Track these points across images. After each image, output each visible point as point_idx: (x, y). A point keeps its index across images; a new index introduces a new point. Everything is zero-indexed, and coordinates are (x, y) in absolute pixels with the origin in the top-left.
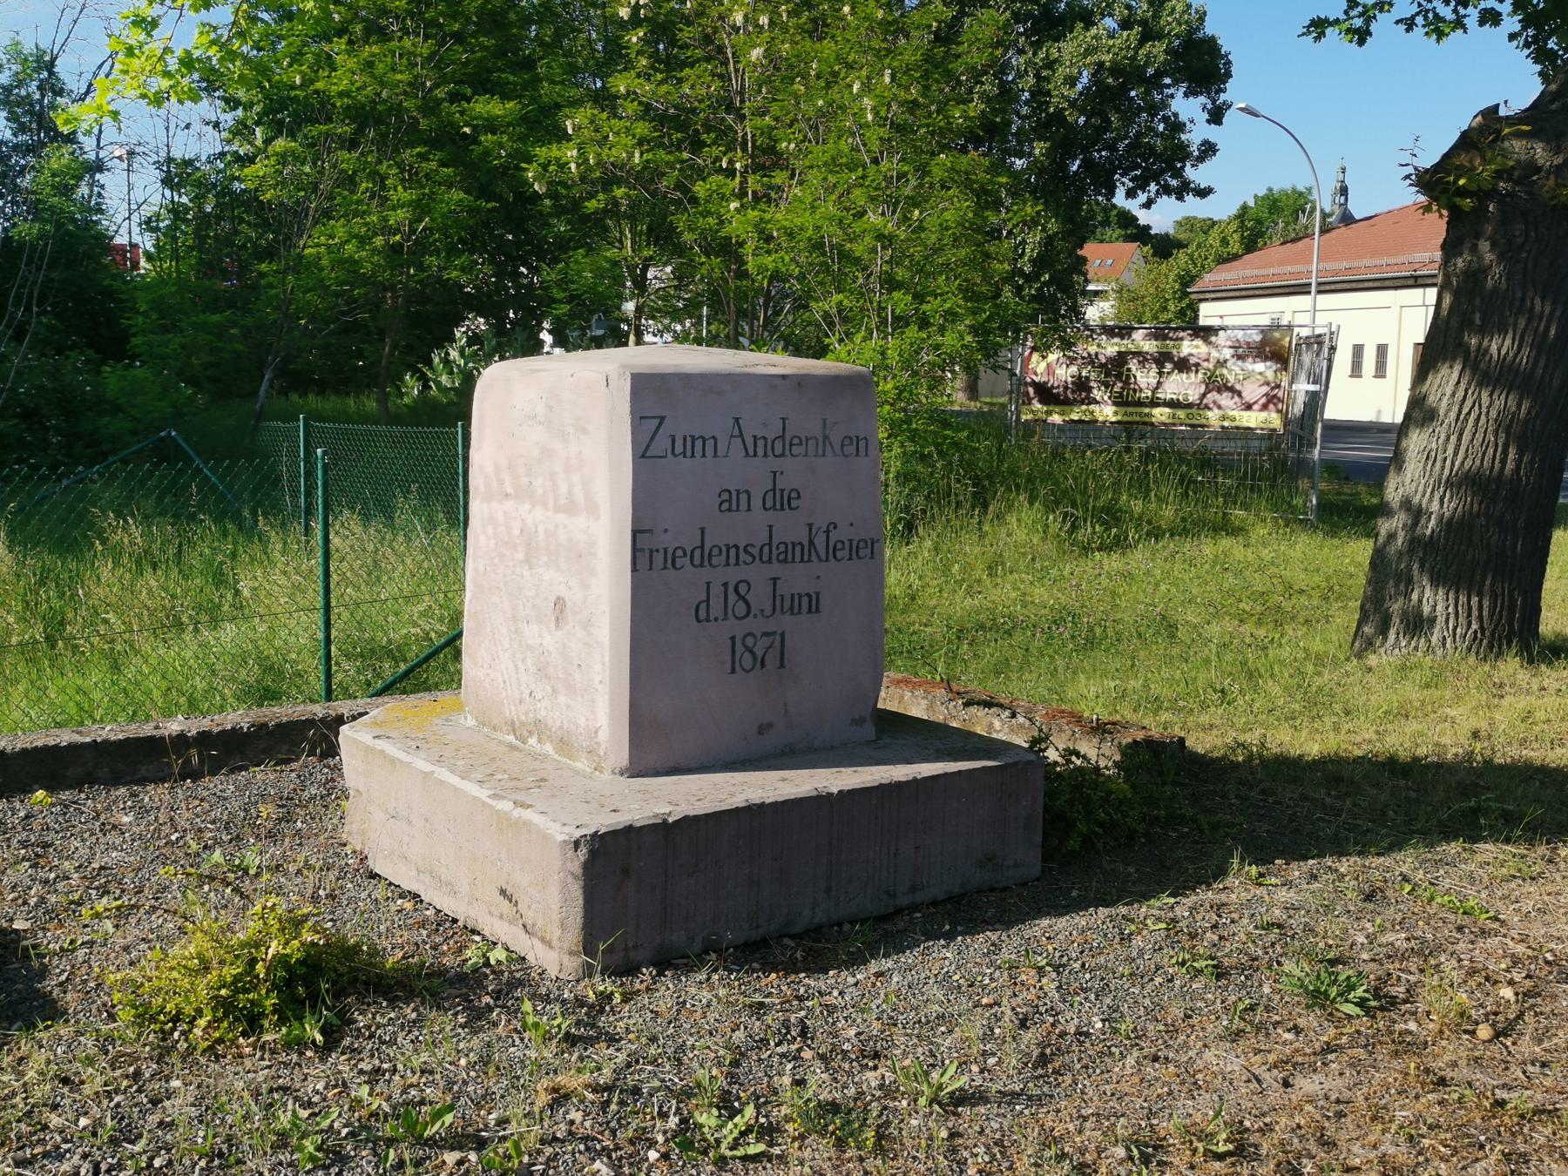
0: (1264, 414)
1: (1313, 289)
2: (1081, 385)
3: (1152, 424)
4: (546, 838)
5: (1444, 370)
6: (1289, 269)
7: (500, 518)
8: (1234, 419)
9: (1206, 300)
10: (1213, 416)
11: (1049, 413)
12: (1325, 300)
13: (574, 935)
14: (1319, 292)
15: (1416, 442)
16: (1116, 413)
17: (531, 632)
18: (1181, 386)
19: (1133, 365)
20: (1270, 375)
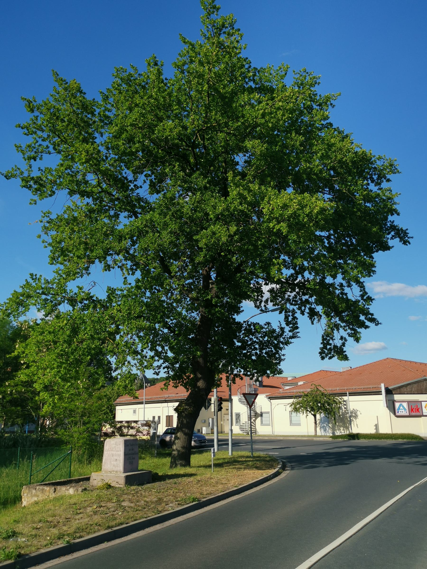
10: (138, 437)
12: (147, 406)
14: (145, 404)
17: (113, 463)
20: (148, 429)
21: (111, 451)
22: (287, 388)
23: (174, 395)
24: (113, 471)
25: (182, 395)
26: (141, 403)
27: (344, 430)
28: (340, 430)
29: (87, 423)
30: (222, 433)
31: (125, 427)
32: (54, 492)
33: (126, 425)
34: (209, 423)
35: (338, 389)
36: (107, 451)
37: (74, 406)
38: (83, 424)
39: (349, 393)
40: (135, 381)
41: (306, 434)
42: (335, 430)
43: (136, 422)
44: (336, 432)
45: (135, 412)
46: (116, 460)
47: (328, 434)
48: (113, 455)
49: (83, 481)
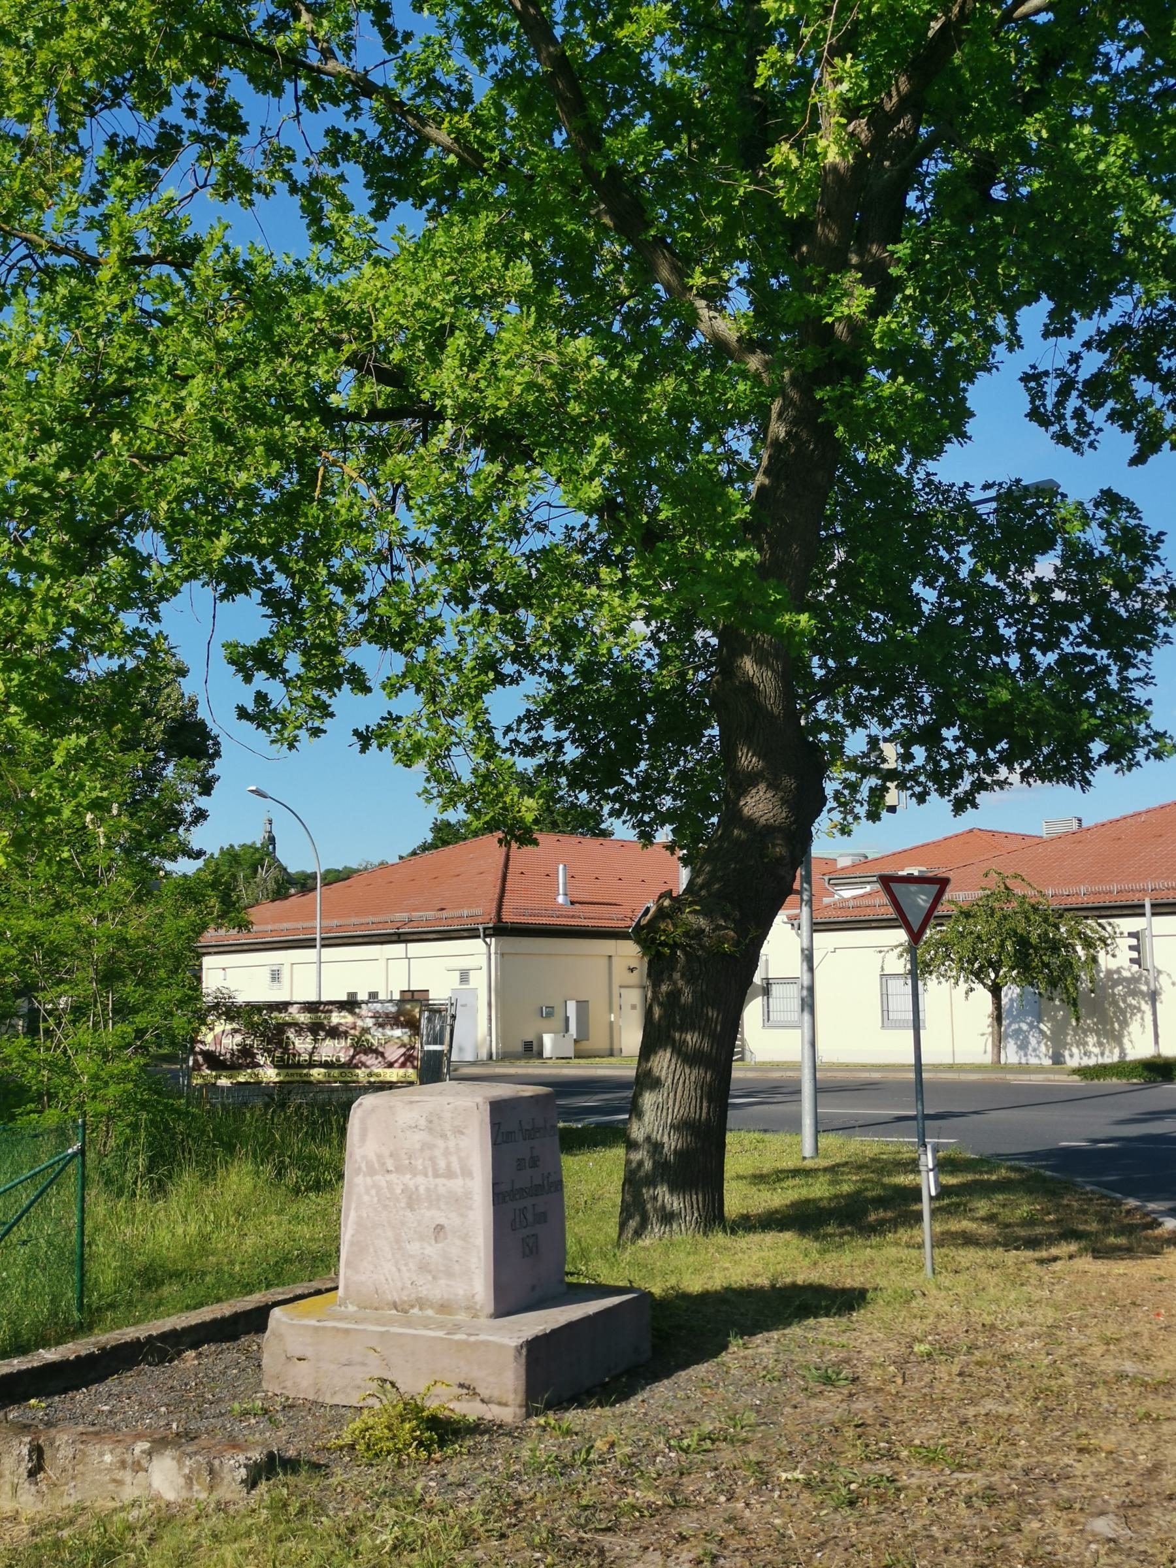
0: (402, 1071)
1: (318, 943)
2: (246, 1052)
3: (311, 1083)
4: (501, 1347)
5: (661, 1053)
6: (285, 925)
7: (384, 1184)
8: (378, 1075)
9: (209, 954)
10: (361, 1073)
11: (218, 1077)
12: (329, 953)
13: (520, 1397)
14: (323, 946)
15: (649, 1099)
16: (278, 1075)
17: (414, 1248)
18: (331, 1049)
19: (291, 1034)
20: (406, 1039)
21: (399, 1170)
22: (847, 893)
23: (431, 914)
24: (421, 1303)
25: (466, 913)
26: (308, 944)
27: (1100, 1044)
28: (1085, 1044)
29: (135, 1010)
30: (611, 1055)
31: (299, 1028)
32: (32, 1473)
33: (304, 1018)
34: (567, 1019)
35: (1083, 893)
36: (372, 1172)
37: (70, 932)
38: (115, 1011)
39: (1153, 905)
40: (256, 871)
41: (948, 1060)
42: (1065, 1045)
43: (350, 1005)
44: (1067, 1053)
45: (275, 976)
46: (439, 1228)
47: (1033, 1061)
48: (412, 1200)
49: (195, 1346)
